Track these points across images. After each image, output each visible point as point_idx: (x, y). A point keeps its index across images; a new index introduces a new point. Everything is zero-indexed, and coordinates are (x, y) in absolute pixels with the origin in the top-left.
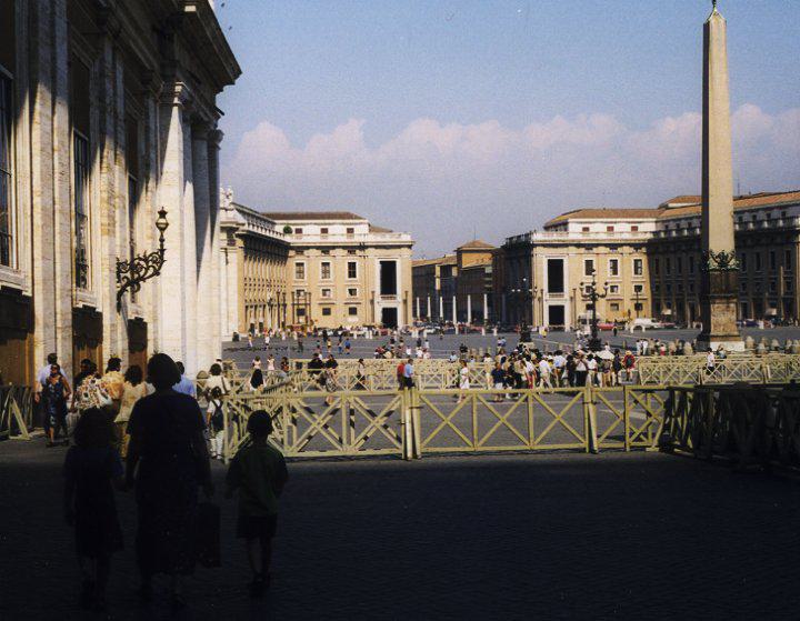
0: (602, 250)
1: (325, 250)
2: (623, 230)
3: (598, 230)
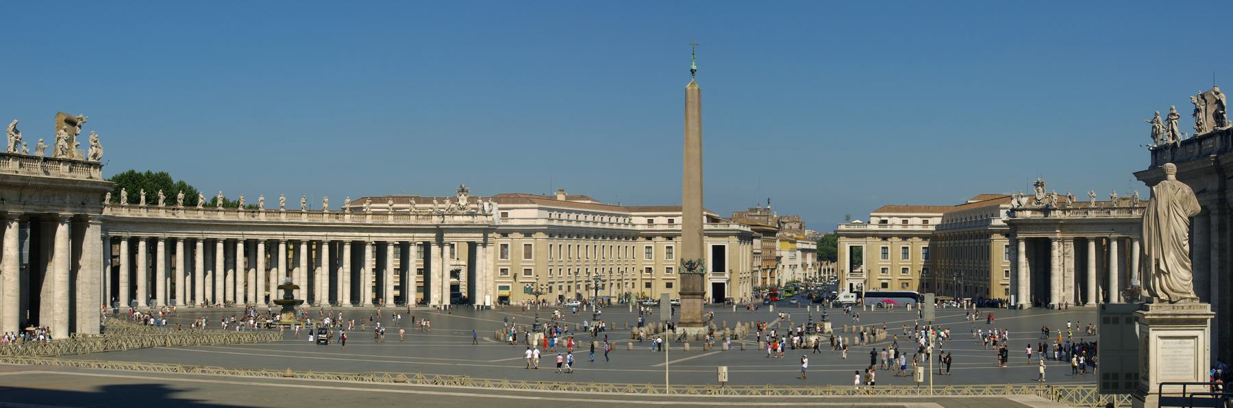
0: (895, 239)
1: (905, 237)
2: (916, 223)
3: (895, 223)
